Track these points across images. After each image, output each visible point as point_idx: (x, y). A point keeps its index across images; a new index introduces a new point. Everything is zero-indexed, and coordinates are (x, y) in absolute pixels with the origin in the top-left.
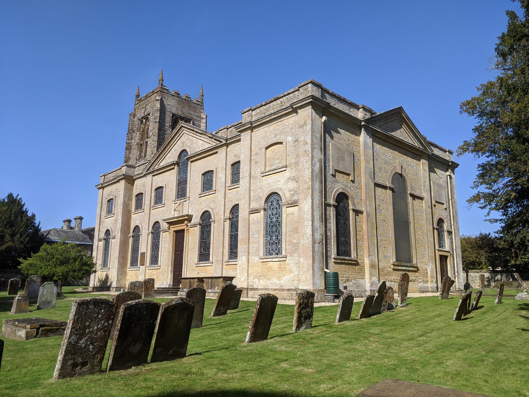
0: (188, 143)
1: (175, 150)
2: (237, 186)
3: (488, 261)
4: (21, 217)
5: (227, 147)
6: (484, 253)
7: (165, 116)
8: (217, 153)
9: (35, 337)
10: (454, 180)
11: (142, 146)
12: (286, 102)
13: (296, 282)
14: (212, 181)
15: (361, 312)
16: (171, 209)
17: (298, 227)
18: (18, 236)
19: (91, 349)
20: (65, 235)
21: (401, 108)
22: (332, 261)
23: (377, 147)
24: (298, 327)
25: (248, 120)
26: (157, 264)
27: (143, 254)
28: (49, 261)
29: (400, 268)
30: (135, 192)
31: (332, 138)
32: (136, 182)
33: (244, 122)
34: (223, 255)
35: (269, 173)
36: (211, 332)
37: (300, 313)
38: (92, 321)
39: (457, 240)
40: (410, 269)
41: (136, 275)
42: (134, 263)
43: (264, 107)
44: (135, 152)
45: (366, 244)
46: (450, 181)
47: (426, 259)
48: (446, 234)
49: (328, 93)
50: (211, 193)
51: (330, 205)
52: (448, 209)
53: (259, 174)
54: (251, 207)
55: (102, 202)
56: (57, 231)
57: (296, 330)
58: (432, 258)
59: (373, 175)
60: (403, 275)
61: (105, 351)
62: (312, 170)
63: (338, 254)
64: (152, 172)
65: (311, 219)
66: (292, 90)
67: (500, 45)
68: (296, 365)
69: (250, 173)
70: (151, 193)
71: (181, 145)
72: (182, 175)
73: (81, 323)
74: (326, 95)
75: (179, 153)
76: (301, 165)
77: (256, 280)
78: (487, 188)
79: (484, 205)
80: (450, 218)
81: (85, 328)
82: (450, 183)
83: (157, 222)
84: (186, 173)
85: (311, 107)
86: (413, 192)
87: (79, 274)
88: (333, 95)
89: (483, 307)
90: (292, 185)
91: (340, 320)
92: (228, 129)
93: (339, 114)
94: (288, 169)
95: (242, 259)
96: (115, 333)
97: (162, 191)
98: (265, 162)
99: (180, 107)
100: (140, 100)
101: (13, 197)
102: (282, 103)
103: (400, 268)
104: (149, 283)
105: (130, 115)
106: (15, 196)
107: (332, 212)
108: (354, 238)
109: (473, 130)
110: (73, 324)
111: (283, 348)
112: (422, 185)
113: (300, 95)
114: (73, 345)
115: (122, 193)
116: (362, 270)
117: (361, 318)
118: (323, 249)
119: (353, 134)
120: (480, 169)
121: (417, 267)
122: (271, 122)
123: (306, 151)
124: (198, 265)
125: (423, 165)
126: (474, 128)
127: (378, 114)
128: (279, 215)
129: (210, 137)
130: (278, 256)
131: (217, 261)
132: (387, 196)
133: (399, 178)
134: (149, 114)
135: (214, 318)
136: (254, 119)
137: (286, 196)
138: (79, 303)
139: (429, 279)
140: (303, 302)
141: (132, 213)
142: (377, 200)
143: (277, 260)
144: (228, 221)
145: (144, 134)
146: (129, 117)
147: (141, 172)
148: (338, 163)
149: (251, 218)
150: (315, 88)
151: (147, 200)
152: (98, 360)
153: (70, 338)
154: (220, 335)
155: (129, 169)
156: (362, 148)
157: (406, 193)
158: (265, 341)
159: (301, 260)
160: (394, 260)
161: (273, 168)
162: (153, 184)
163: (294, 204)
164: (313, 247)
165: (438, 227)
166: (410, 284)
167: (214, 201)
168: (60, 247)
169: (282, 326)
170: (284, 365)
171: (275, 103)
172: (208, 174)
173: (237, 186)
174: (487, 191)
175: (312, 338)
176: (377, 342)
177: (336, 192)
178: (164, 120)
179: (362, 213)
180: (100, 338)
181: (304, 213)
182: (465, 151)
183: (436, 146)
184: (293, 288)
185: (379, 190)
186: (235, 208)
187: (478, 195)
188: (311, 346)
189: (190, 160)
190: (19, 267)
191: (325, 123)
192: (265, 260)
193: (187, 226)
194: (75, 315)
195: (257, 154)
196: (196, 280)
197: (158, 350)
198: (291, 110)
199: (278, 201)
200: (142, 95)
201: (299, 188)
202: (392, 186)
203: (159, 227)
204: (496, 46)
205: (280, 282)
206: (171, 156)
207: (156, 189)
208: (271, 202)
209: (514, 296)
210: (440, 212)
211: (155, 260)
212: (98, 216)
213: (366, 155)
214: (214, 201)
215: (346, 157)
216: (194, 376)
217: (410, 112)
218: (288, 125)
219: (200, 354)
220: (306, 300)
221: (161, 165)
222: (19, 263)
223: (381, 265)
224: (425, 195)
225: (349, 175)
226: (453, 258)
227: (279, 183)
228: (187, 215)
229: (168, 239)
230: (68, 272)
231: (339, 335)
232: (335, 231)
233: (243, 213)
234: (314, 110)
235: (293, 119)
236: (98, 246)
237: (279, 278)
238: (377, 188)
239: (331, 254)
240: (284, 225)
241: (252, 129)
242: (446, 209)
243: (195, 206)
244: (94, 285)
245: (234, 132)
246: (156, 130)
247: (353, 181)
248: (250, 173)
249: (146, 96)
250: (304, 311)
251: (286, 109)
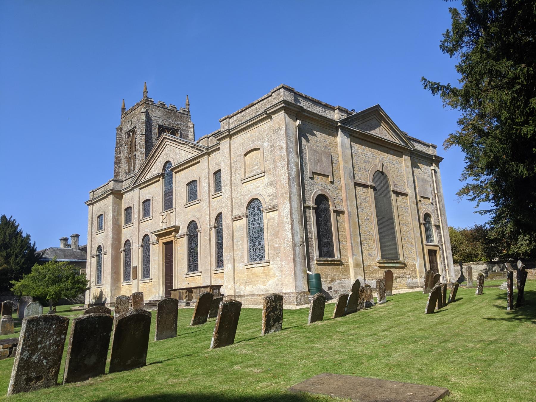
0: (171, 154)
1: (160, 162)
2: (220, 194)
3: (485, 253)
4: (16, 239)
5: (209, 156)
6: (474, 246)
7: (151, 128)
8: (199, 162)
9: (8, 356)
10: (439, 174)
11: (131, 159)
12: (260, 108)
13: (280, 286)
14: (196, 190)
15: (335, 311)
16: (159, 221)
17: (278, 232)
18: (13, 257)
19: (45, 364)
20: (61, 253)
22: (314, 263)
23: (356, 146)
24: (267, 330)
25: (226, 127)
26: (149, 277)
27: (135, 268)
28: (41, 281)
29: (386, 265)
30: (124, 206)
31: (308, 140)
32: (125, 196)
33: (222, 130)
34: (211, 264)
35: (249, 179)
36: (183, 340)
37: (268, 317)
38: (44, 336)
39: (445, 234)
40: (397, 265)
41: (127, 289)
42: (127, 277)
43: (240, 114)
44: (124, 166)
45: (349, 244)
46: (435, 175)
47: (414, 255)
48: (433, 228)
49: (301, 96)
50: (196, 203)
51: (309, 208)
52: (434, 204)
53: (240, 181)
54: (234, 215)
55: (92, 218)
56: (54, 250)
57: (265, 333)
58: (420, 254)
59: (352, 174)
60: (386, 272)
61: (60, 364)
62: (289, 174)
63: (320, 255)
64: (138, 185)
66: (266, 96)
67: (445, 42)
68: (247, 367)
69: (231, 180)
70: (139, 206)
72: (168, 187)
73: (32, 339)
74: (299, 98)
75: (163, 165)
76: (278, 170)
77: (243, 287)
78: (474, 179)
79: (473, 196)
80: (437, 212)
81: (37, 343)
82: (436, 178)
83: (146, 235)
85: (284, 111)
86: (397, 189)
87: (72, 292)
88: (306, 98)
89: (462, 299)
90: (271, 190)
91: (313, 320)
92: (208, 138)
93: (314, 117)
94: (266, 174)
95: (228, 266)
96: (68, 348)
97: (150, 204)
98: (245, 169)
99: (166, 117)
100: (126, 113)
101: (7, 219)
102: (257, 109)
103: (386, 265)
104: (138, 297)
105: (117, 129)
106: (8, 217)
107: (311, 215)
108: (336, 239)
109: (457, 122)
110: (24, 341)
111: (244, 351)
112: (406, 181)
113: (274, 100)
114: (25, 361)
115: (111, 208)
116: (347, 269)
117: (335, 318)
118: (304, 251)
119: (329, 135)
120: (467, 161)
121: (404, 263)
122: (247, 129)
123: (281, 156)
124: (188, 276)
125: (405, 161)
126: (458, 120)
128: (260, 221)
129: (192, 147)
130: (262, 261)
131: (205, 270)
132: (369, 195)
133: (381, 176)
134: (135, 127)
135: (193, 327)
136: (232, 126)
137: (266, 202)
138: (28, 321)
139: (418, 274)
140: (270, 305)
141: (123, 228)
142: (358, 200)
143: (261, 265)
144: (214, 229)
145: (132, 148)
146: (116, 131)
148: (316, 165)
149: (234, 226)
150: (287, 93)
151: (136, 213)
152: (53, 374)
153: (22, 353)
154: (190, 343)
155: (116, 183)
156: (340, 149)
157: (388, 190)
158: (229, 347)
159: (284, 263)
160: (380, 258)
161: (252, 174)
162: (141, 197)
163: (273, 209)
164: (294, 250)
165: (425, 222)
167: (199, 210)
168: (51, 267)
169: (254, 330)
170: (237, 367)
171: (250, 109)
172: (192, 184)
174: (475, 183)
175: (277, 340)
176: (339, 339)
177: (315, 194)
178: (151, 132)
179: (343, 213)
180: (54, 353)
181: (284, 217)
182: (452, 144)
183: (418, 142)
185: (360, 189)
186: (219, 216)
187: (467, 187)
188: (272, 347)
189: (174, 171)
190: (12, 290)
191: (299, 127)
192: (249, 266)
193: (175, 237)
194: (26, 332)
196: (185, 291)
197: (116, 361)
198: (265, 116)
199: (259, 207)
200: (128, 108)
201: (277, 192)
202: (373, 185)
203: (149, 240)
204: (441, 43)
205: (264, 287)
206: (156, 169)
207: (144, 202)
209: (498, 286)
210: (426, 207)
211: (146, 273)
212: (90, 233)
213: (344, 155)
214: (199, 210)
215: (324, 159)
216: (144, 383)
217: (388, 109)
218: (264, 131)
219: (161, 362)
220: (275, 303)
221: (147, 177)
222: (12, 285)
223: (366, 263)
224: (410, 191)
225: (328, 176)
226: (443, 252)
227: (258, 189)
228: (174, 227)
229: (157, 251)
230: (60, 291)
231: (304, 335)
232: (316, 232)
233: (226, 222)
234: (287, 114)
235: (268, 125)
236: (91, 262)
237: (264, 284)
238: (357, 188)
239: (313, 256)
240: (265, 230)
241: (230, 136)
242: (432, 203)
243: (180, 217)
244: (90, 302)
245: (213, 141)
246: (144, 142)
247: (332, 183)
248: (231, 180)
249: (132, 109)
250: (273, 314)
251: (261, 115)
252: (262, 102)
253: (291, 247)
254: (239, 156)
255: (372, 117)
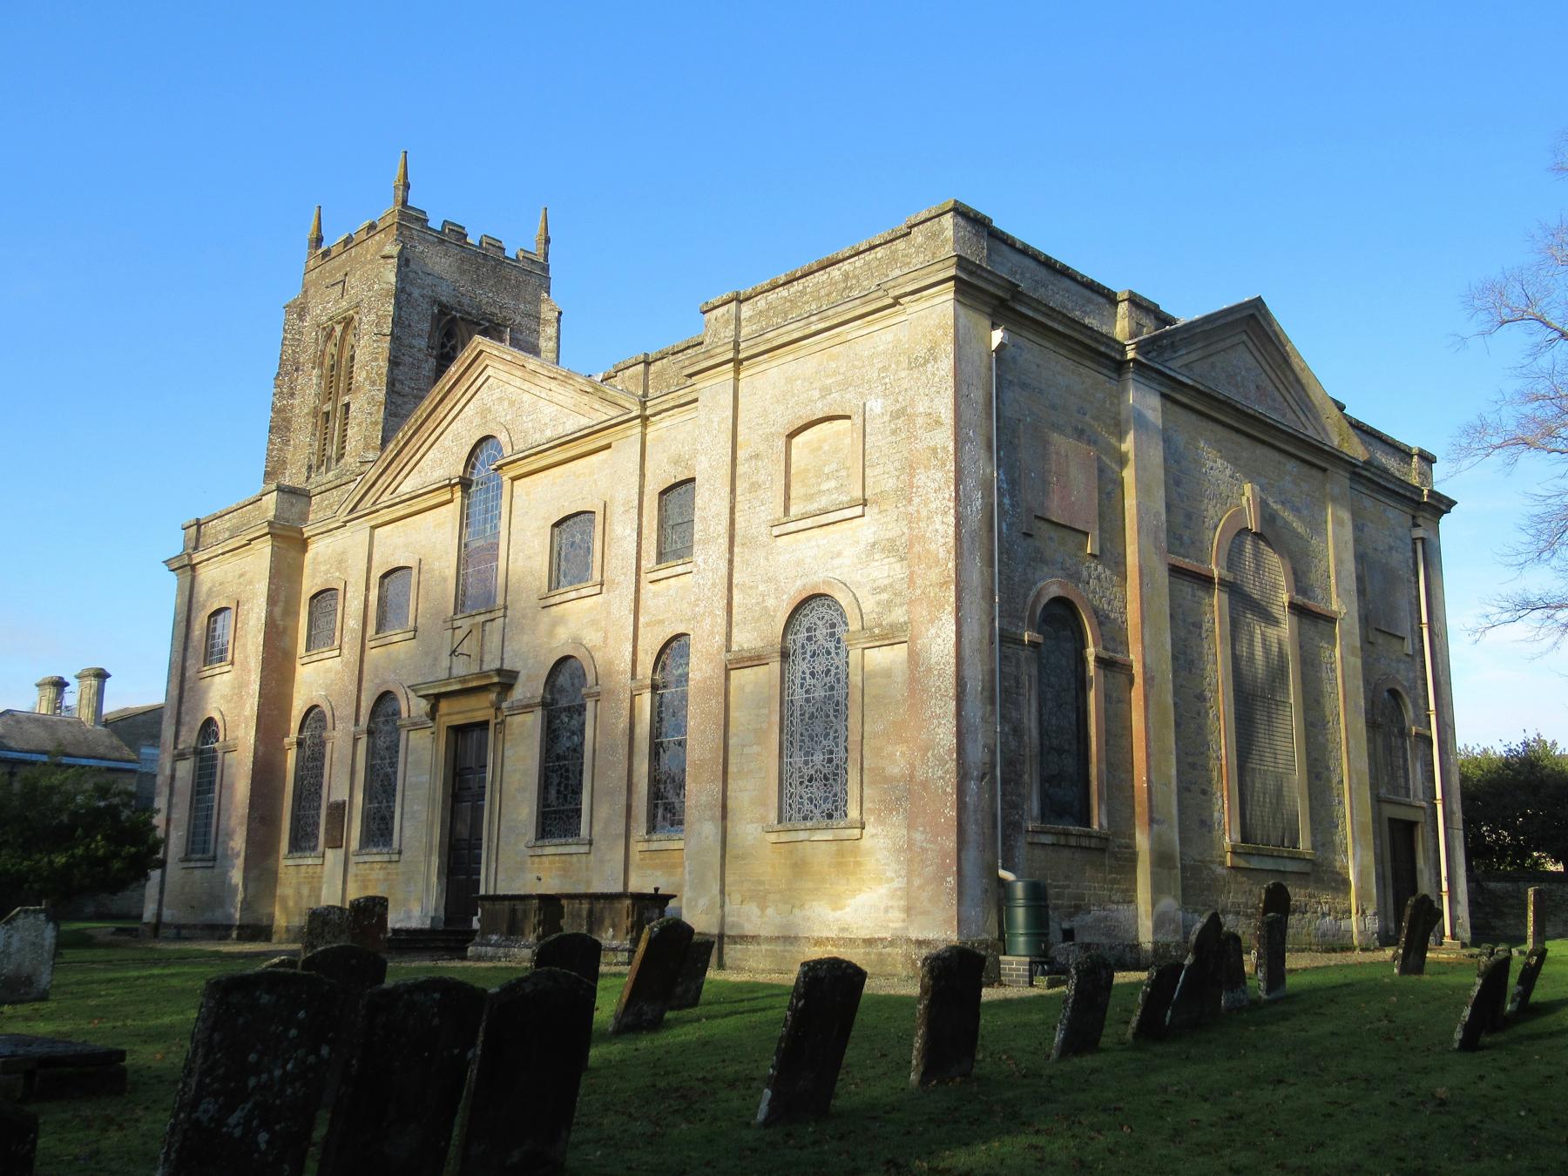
1: (457, 437)
2: (680, 569)
8: (608, 446)
11: (331, 421)
14: (589, 550)
19: (263, 1147)
21: (1258, 303)
27: (338, 812)
42: (302, 840)
44: (303, 440)
50: (584, 592)
53: (764, 529)
65: (952, 692)
70: (367, 589)
71: (477, 421)
75: (468, 449)
76: (916, 500)
84: (492, 515)
90: (886, 570)
92: (648, 364)
94: (871, 511)
100: (326, 254)
102: (846, 277)
115: (262, 587)
118: (993, 798)
123: (934, 451)
127: (1179, 324)
141: (298, 662)
145: (338, 376)
147: (329, 513)
161: (813, 507)
162: (376, 557)
166: (1293, 920)
171: (820, 277)
173: (680, 569)
184: (887, 935)
195: (757, 456)
199: (833, 626)
200: (332, 240)
203: (397, 713)
206: (441, 458)
208: (809, 630)
211: (379, 830)
227: (836, 562)
246: (384, 365)
252: (868, 256)
253: (952, 778)
254: (767, 439)
255: (1236, 340)
